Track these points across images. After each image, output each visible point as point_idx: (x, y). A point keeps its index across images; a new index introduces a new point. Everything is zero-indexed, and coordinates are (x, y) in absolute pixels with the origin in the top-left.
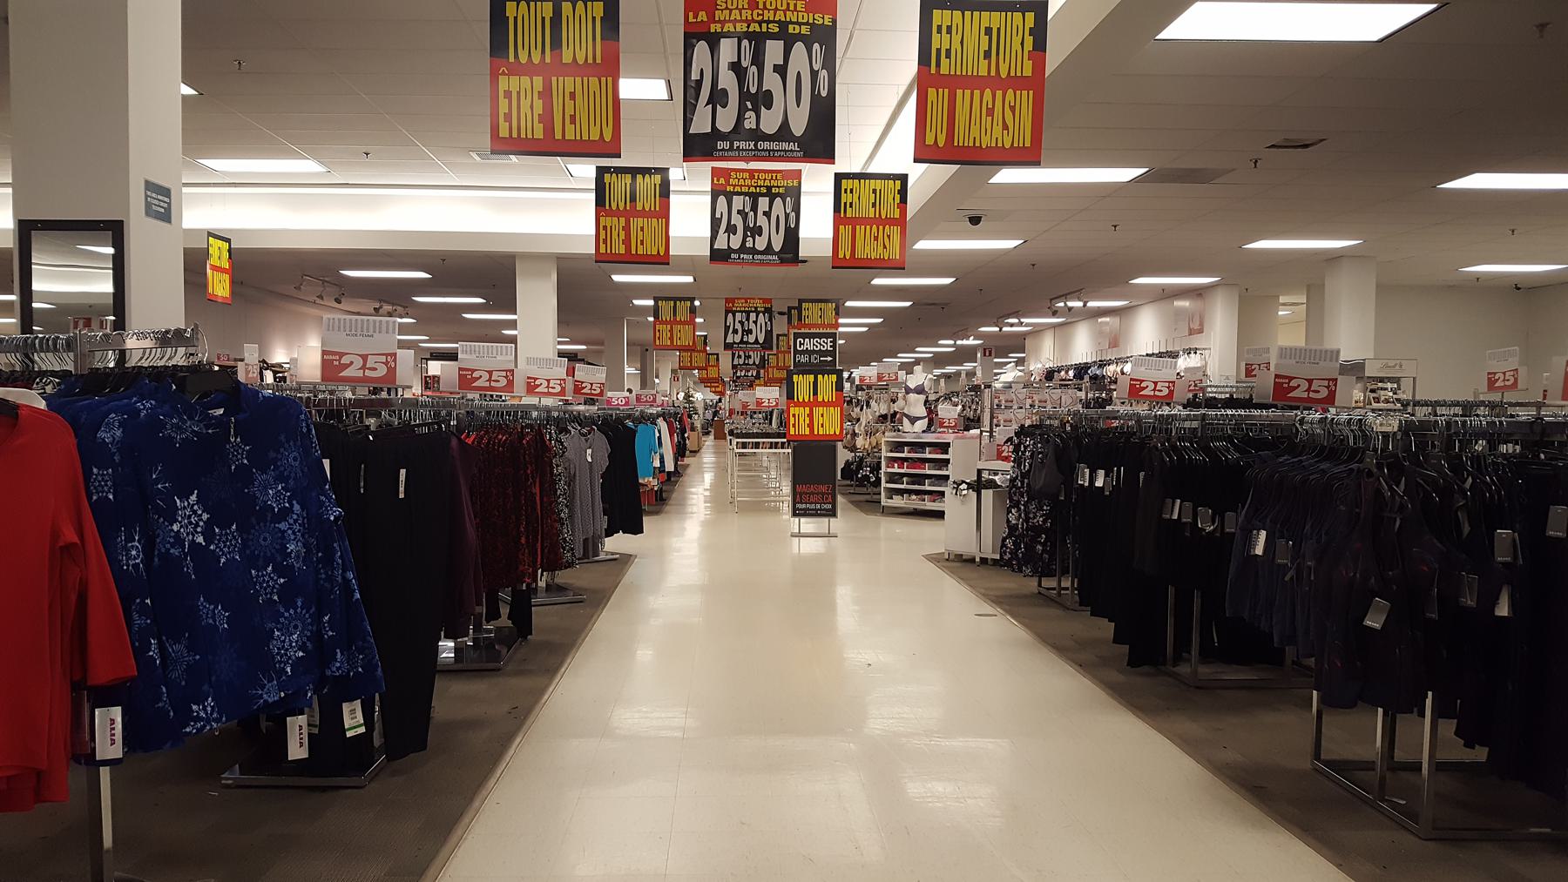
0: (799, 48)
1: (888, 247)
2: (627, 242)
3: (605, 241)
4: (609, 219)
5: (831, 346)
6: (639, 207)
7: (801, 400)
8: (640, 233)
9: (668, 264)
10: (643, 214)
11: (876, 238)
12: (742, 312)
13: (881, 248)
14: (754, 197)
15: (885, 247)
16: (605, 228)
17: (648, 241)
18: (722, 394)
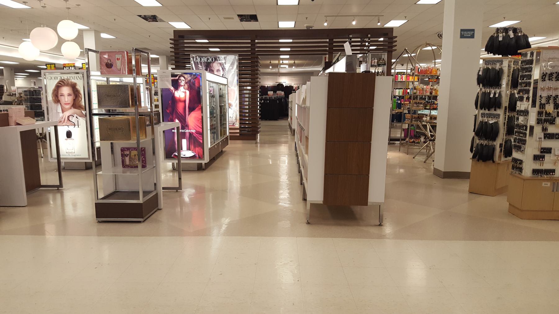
12: (68, 67)
14: (69, 67)
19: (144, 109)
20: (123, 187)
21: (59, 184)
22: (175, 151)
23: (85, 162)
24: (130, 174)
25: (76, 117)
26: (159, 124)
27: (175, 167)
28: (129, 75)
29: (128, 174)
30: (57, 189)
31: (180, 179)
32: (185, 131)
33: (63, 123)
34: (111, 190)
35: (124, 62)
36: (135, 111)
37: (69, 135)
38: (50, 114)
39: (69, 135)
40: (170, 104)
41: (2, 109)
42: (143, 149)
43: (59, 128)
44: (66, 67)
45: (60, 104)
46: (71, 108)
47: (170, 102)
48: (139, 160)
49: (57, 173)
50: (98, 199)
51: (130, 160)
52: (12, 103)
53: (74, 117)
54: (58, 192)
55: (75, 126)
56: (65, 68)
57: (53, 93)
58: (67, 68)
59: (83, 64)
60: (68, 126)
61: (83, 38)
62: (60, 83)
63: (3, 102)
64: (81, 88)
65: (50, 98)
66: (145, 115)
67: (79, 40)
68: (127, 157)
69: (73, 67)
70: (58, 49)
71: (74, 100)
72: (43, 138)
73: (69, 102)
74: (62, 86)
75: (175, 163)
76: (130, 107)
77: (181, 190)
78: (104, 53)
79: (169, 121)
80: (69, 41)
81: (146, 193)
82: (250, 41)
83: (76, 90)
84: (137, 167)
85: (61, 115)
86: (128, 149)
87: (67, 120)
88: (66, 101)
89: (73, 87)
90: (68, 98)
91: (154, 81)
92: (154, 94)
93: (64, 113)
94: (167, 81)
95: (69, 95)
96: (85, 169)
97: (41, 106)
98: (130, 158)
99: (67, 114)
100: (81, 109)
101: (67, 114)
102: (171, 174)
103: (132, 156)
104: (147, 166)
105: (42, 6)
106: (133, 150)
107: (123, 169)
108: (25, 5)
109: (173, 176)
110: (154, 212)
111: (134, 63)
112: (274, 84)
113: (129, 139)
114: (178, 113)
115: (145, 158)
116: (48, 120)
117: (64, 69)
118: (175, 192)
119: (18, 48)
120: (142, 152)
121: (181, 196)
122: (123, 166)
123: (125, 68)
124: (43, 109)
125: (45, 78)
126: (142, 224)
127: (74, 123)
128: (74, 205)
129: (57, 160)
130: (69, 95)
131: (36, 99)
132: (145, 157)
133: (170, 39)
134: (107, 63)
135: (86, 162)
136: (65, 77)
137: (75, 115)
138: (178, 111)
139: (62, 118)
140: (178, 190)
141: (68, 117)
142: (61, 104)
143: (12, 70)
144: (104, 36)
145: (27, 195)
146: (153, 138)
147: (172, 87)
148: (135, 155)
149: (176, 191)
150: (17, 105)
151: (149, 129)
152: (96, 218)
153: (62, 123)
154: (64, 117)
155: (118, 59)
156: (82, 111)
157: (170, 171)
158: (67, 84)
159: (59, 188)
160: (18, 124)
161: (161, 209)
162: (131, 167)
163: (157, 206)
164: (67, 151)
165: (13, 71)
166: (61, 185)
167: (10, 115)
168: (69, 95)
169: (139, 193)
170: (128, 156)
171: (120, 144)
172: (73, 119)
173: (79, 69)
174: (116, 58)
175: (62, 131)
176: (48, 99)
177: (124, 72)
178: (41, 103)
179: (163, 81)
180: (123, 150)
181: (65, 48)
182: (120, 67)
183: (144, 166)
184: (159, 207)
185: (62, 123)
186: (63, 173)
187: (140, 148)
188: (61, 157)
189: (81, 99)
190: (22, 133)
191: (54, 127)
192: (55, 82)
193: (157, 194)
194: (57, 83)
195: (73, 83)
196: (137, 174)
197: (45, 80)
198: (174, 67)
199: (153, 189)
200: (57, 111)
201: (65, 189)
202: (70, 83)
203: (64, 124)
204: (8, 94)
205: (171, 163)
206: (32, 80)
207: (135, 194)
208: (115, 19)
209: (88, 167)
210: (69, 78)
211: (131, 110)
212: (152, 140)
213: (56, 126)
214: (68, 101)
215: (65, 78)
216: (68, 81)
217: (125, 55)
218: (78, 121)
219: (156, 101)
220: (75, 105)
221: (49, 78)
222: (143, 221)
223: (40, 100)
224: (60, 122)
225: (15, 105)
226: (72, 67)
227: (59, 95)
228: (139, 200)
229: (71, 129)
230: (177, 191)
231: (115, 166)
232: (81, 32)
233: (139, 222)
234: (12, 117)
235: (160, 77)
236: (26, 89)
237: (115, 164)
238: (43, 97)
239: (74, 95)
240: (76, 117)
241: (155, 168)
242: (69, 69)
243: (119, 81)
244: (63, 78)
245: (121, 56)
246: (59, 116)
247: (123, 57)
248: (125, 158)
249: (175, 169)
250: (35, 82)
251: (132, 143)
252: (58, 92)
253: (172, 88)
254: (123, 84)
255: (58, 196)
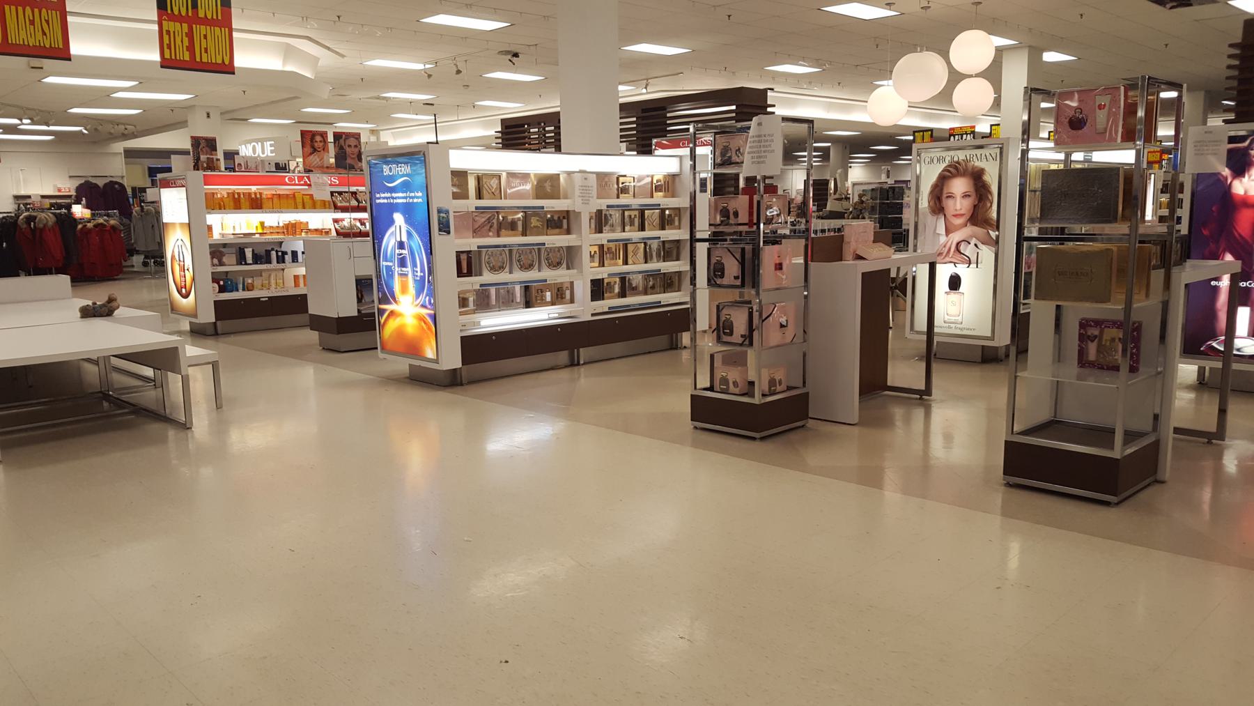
0: (969, 135)
1: (47, 31)
2: (191, 49)
3: (169, 47)
4: (172, 23)
5: (272, 152)
6: (201, 14)
7: (176, 12)
8: (204, 41)
9: (234, 73)
10: (205, 21)
11: (32, 23)
12: (958, 135)
13: (39, 35)
14: (962, 135)
15: (44, 34)
16: (168, 32)
17: (212, 50)
18: (392, 208)
19: (1149, 226)
20: (1074, 414)
21: (923, 388)
22: (1214, 336)
23: (983, 346)
24: (1099, 385)
25: (976, 245)
26: (1181, 264)
27: (1206, 379)
28: (1124, 143)
29: (1091, 383)
30: (920, 399)
31: (1222, 412)
32: (1250, 284)
33: (945, 256)
34: (1044, 415)
35: (1116, 114)
36: (1130, 231)
37: (955, 283)
38: (920, 238)
39: (955, 283)
40: (1215, 214)
41: (826, 228)
42: (1135, 326)
43: (939, 267)
44: (954, 136)
45: (943, 216)
46: (966, 226)
47: (1214, 209)
48: (1124, 351)
49: (923, 365)
50: (695, 388)
51: (1098, 351)
52: (844, 215)
53: (970, 243)
54: (921, 405)
55: (970, 264)
56: (952, 138)
57: (932, 192)
58: (957, 137)
59: (993, 127)
60: (955, 263)
61: (1001, 68)
62: (949, 171)
63: (828, 213)
64: (993, 179)
65: (924, 203)
66: (1149, 242)
67: (993, 74)
68: (1092, 341)
69: (970, 134)
70: (945, 96)
71: (975, 206)
72: (896, 288)
73: (962, 212)
74: (954, 176)
75: (1207, 368)
76: (1116, 222)
77: (1224, 440)
78: (1069, 95)
79: (1205, 258)
80: (971, 76)
81: (1130, 436)
82: (635, 119)
83: (981, 184)
84: (1116, 368)
85: (943, 239)
86: (1098, 323)
87: (954, 252)
88: (956, 210)
89: (977, 177)
90: (961, 203)
91: (1161, 156)
92: (1162, 190)
93: (950, 236)
94: (1215, 154)
95: (966, 196)
96: (980, 360)
97: (902, 220)
98: (1100, 346)
99: (956, 237)
100: (988, 227)
101: (956, 237)
102: (1192, 395)
103: (1106, 340)
104: (1141, 369)
105: (922, 8)
106: (1109, 327)
107: (1079, 369)
108: (890, 10)
109: (1198, 402)
110: (1141, 487)
111: (1141, 113)
112: (1031, 174)
113: (1106, 300)
114: (1235, 237)
115: (1138, 350)
116: (915, 251)
117: (949, 140)
118: (1204, 443)
119: (867, 102)
120: (1132, 334)
121: (1219, 457)
122: (1078, 364)
123: (1117, 126)
124: (904, 227)
125: (919, 162)
126: (757, 443)
127: (968, 257)
128: (948, 438)
129: (926, 336)
130: (965, 196)
131: (892, 207)
132: (1137, 347)
133: (1231, 46)
134: (1073, 116)
135: (983, 347)
136: (960, 156)
137: (973, 241)
138: (1237, 231)
139: (945, 246)
140: (1214, 441)
141: (958, 244)
142: (945, 215)
143: (846, 148)
144: (1050, 57)
145: (860, 402)
146: (1166, 299)
147: (1227, 170)
148: (1113, 340)
149: (1208, 442)
150: (852, 218)
151: (1157, 276)
152: (692, 420)
153: (942, 257)
154: (950, 243)
155: (1101, 107)
156: (990, 232)
157: (1190, 388)
158: (964, 173)
159: (923, 397)
160: (860, 258)
161: (1163, 482)
162: (1099, 368)
163: (1155, 472)
164: (947, 318)
165: (848, 151)
166: (928, 391)
167: (846, 239)
168: (966, 196)
169: (1114, 433)
170: (1096, 340)
171: (1078, 311)
172: (968, 250)
173: (983, 138)
174: (1097, 104)
175: (944, 272)
176: (920, 207)
177: (1114, 135)
178: (902, 214)
179: (1202, 154)
180: (1084, 324)
181: (962, 93)
182: (1105, 126)
183: (1133, 369)
184: (1159, 476)
185: (942, 257)
186: (934, 366)
187: (1131, 323)
188: (936, 330)
189: (991, 203)
190: (866, 276)
191: (928, 265)
192: (938, 169)
193: (1156, 444)
194: (943, 171)
195: (976, 169)
196: (1115, 386)
197: (918, 165)
198: (1232, 116)
199: (1150, 428)
200: (935, 230)
201: (935, 400)
202: (970, 169)
203: (947, 259)
204: (837, 196)
205: (1195, 368)
206: (883, 167)
207: (1103, 435)
208: (1082, 15)
209: (987, 357)
210: (968, 158)
211: (1122, 228)
212: (1161, 305)
213: (933, 263)
214: (961, 209)
215: (960, 158)
216: (966, 166)
217: (1120, 95)
218: (978, 253)
219: (1163, 206)
220: (977, 217)
221: (928, 160)
222: (1116, 502)
223: (899, 208)
224: (940, 254)
225: (848, 219)
226: (967, 134)
227: (945, 196)
228: (1112, 448)
229: (961, 270)
230: (1209, 442)
231: (1059, 361)
232: (1000, 51)
233: (1107, 504)
234: (849, 243)
235: (1195, 146)
236: (873, 186)
237: (1059, 357)
238: (908, 199)
239: (977, 195)
240: (976, 245)
241: (1162, 375)
242: (962, 139)
243: (1082, 159)
244: (956, 159)
245: (1109, 100)
246: (939, 242)
247: (1115, 101)
248: (1086, 345)
249: (1206, 384)
250: (889, 171)
251: (1113, 308)
252: (942, 190)
253: (1226, 172)
254: (1092, 166)
255: (919, 413)
